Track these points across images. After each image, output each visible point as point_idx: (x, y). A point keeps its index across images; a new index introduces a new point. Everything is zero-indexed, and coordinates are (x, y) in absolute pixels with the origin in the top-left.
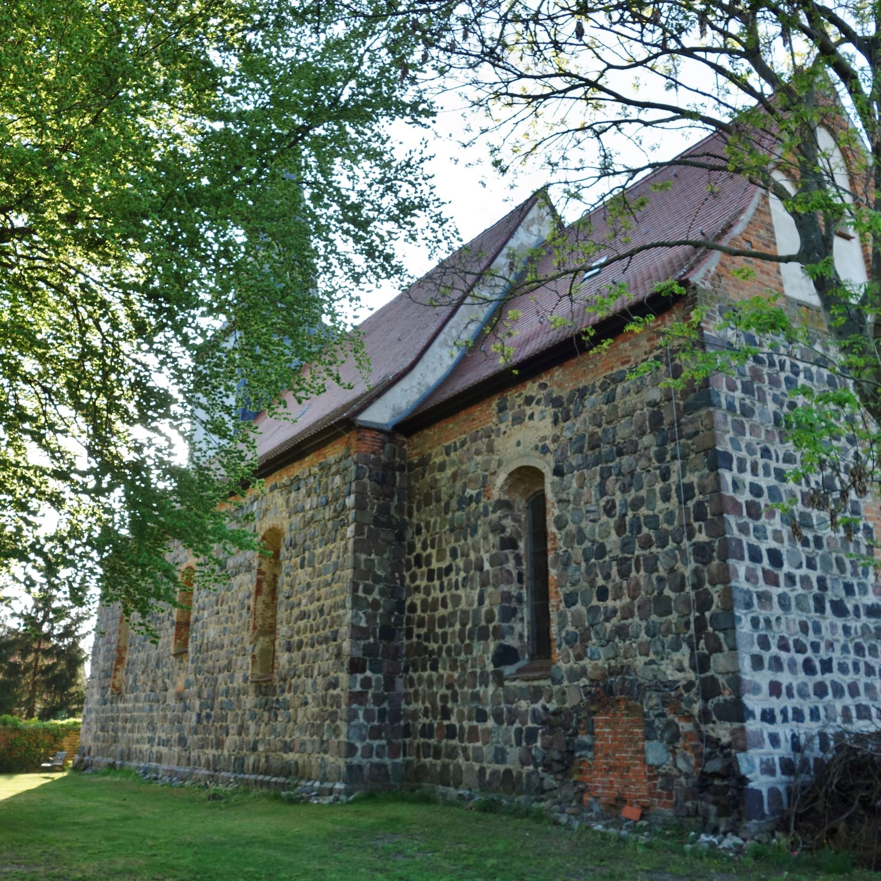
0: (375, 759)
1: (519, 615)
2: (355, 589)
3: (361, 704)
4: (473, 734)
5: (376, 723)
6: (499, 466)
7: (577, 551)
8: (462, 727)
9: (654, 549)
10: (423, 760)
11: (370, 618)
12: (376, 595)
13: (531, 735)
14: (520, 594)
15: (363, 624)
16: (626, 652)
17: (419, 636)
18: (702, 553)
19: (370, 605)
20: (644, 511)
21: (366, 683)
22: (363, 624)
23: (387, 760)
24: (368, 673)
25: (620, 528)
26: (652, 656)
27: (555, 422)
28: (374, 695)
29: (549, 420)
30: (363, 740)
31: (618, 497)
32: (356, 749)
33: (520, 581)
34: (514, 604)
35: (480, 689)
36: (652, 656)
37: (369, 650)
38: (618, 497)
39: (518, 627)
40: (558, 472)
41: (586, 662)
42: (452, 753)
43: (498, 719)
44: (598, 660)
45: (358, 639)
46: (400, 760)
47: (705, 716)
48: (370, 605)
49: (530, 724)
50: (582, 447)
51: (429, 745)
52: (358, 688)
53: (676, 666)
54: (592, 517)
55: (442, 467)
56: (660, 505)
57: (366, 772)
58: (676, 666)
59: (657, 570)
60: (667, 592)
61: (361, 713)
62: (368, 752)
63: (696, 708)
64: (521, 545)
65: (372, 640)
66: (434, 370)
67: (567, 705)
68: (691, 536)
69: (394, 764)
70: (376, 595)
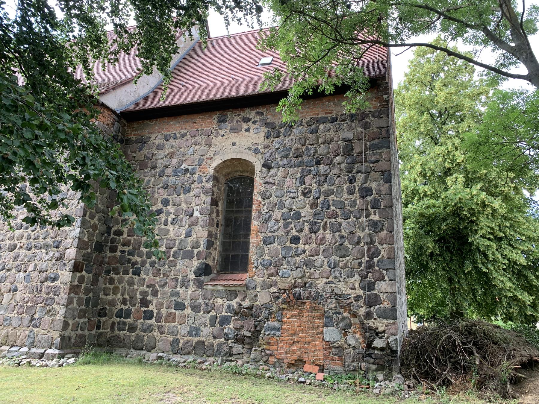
0: (79, 332)
1: (215, 246)
2: (84, 215)
3: (76, 293)
4: (171, 318)
5: (83, 307)
6: (215, 155)
7: (277, 214)
8: (159, 313)
9: (338, 220)
10: (117, 332)
11: (91, 235)
12: (96, 220)
13: (225, 321)
14: (216, 234)
15: (86, 239)
16: (311, 275)
17: (123, 252)
18: (375, 226)
19: (91, 227)
20: (332, 198)
21: (82, 279)
22: (86, 239)
23: (86, 332)
24: (84, 273)
25: (313, 205)
26: (331, 279)
27: (268, 136)
28: (85, 288)
29: (262, 135)
30: (74, 319)
31: (314, 187)
32: (69, 324)
33: (217, 226)
34: (213, 239)
35: (182, 290)
36: (331, 279)
37: (87, 257)
38: (314, 187)
39: (213, 253)
40: (267, 166)
41: (277, 278)
42: (148, 329)
43: (196, 308)
44: (287, 276)
45: (81, 249)
46: (94, 332)
47: (369, 315)
48: (91, 227)
49: (224, 313)
50: (288, 154)
51: (124, 324)
52: (76, 283)
53: (350, 287)
54: (292, 195)
55: (160, 147)
56: (346, 196)
57: (73, 340)
58: (350, 287)
59: (340, 231)
60: (346, 244)
61: (75, 300)
62: (76, 327)
63: (362, 311)
64: (220, 204)
65: (89, 250)
66: (144, 87)
67: (258, 303)
68: (367, 216)
69: (90, 334)
70: (96, 220)
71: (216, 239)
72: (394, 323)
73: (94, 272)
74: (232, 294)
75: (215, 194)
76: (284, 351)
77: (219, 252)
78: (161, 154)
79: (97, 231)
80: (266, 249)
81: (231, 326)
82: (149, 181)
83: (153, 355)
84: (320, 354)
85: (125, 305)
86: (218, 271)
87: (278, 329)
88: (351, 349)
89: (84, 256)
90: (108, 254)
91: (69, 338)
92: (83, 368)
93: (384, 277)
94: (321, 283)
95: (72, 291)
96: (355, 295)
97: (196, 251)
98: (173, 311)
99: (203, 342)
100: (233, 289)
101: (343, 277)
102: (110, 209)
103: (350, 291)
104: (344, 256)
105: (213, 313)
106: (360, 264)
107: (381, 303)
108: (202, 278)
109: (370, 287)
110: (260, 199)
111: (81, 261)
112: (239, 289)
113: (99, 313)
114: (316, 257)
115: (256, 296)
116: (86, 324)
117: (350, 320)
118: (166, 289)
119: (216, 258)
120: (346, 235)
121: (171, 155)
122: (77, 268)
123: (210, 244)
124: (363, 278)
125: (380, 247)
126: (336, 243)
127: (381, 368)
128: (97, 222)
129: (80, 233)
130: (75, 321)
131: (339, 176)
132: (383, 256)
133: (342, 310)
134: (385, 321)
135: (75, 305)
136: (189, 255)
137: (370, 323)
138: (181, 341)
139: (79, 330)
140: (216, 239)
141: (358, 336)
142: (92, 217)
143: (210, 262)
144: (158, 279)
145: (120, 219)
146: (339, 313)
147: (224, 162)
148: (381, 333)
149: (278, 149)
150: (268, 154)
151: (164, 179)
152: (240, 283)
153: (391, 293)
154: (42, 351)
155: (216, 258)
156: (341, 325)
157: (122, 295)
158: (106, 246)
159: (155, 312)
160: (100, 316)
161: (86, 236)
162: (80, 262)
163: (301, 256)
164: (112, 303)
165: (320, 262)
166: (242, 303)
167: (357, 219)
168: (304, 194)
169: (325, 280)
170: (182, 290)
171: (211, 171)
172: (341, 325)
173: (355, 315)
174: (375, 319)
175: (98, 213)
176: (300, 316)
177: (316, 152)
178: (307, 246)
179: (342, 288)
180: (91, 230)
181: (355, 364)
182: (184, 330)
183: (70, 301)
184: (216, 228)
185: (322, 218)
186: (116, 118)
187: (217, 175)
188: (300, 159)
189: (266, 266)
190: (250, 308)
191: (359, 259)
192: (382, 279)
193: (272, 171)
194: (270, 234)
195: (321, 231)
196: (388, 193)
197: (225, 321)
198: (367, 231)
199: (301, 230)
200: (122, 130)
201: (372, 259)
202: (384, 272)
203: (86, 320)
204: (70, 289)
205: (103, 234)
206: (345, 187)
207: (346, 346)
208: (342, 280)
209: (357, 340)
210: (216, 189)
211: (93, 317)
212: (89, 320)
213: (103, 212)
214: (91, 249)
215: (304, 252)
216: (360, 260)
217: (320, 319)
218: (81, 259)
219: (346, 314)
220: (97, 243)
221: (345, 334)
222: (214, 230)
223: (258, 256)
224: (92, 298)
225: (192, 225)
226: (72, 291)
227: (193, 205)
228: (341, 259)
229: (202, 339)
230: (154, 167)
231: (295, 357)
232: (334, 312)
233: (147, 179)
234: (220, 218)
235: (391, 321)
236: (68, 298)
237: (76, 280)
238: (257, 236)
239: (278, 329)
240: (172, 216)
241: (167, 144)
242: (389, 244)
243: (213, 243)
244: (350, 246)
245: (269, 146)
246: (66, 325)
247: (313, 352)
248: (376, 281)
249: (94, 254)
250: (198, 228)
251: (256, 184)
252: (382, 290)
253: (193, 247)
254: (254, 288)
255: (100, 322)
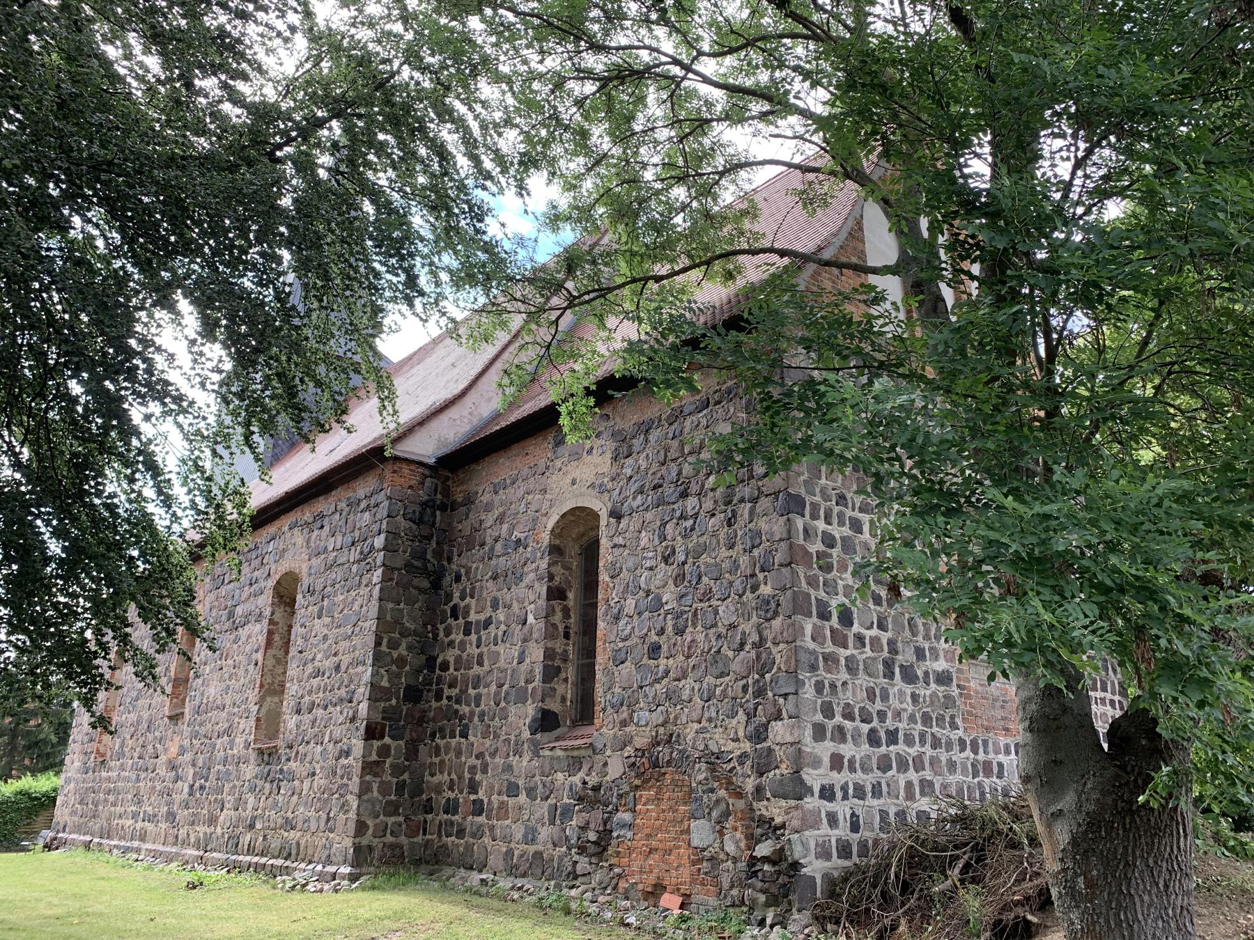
0: (389, 839)
1: (563, 675)
2: (378, 643)
5: (393, 797)
10: (444, 838)
11: (394, 677)
12: (402, 650)
14: (565, 651)
15: (385, 683)
16: (676, 718)
17: (449, 698)
19: (393, 662)
21: (384, 752)
22: (385, 683)
23: (403, 840)
24: (387, 740)
26: (704, 723)
30: (377, 817)
32: (367, 827)
34: (557, 663)
35: (514, 760)
37: (389, 714)
39: (561, 689)
40: (616, 515)
42: (478, 833)
43: (531, 792)
45: (376, 700)
49: (566, 800)
51: (452, 823)
52: (374, 757)
53: (729, 737)
61: (375, 787)
62: (382, 831)
63: (750, 785)
64: (571, 595)
65: (394, 702)
68: (755, 588)
70: (402, 650)
71: (565, 661)
72: (796, 807)
73: (407, 736)
74: (574, 764)
75: (557, 578)
76: (640, 870)
77: (575, 684)
78: (489, 519)
79: (408, 668)
80: (616, 674)
81: (574, 823)
82: (477, 568)
83: (476, 877)
84: (686, 873)
85: (453, 791)
86: (572, 722)
87: (630, 826)
88: (729, 862)
89: (384, 711)
90: (434, 704)
91: (370, 848)
92: (360, 894)
93: (780, 711)
94: (690, 731)
95: (367, 770)
96: (739, 753)
97: (530, 687)
98: (506, 798)
99: (541, 853)
100: (576, 753)
101: (721, 717)
102: (429, 627)
103: (731, 746)
104: (722, 675)
105: (551, 801)
106: (745, 689)
107: (777, 767)
108: (538, 736)
109: (759, 735)
110: (607, 579)
111: (379, 720)
112: (583, 753)
113: (425, 806)
114: (683, 682)
115: (605, 764)
116: (400, 825)
117: (728, 804)
118: (497, 760)
119: (569, 696)
120: (724, 631)
121: (501, 519)
122: (372, 733)
123: (551, 673)
124: (750, 716)
125: (774, 650)
126: (710, 649)
127: (773, 901)
128: (405, 653)
129: (372, 675)
130: (378, 821)
131: (713, 515)
132: (779, 668)
133: (716, 784)
134: (783, 803)
135: (376, 793)
136: (522, 699)
137: (762, 808)
138: (516, 853)
139: (388, 835)
140: (565, 661)
141: (738, 835)
142: (394, 645)
143: (554, 706)
144: (488, 742)
145: (446, 640)
146: (712, 791)
147: (563, 516)
148: (779, 829)
149: (631, 477)
150: (617, 491)
151: (493, 562)
152: (585, 741)
153: (792, 744)
154: (88, 838)
155: (569, 696)
156: (715, 814)
157: (449, 775)
158: (429, 691)
159: (486, 801)
160: (427, 813)
161: (386, 678)
162: (377, 723)
163: (664, 682)
164: (438, 789)
165: (687, 692)
166: (587, 779)
167: (740, 596)
168: (666, 559)
169: (696, 726)
170: (514, 760)
171: (545, 538)
172: (715, 814)
173: (739, 795)
174: (768, 799)
175: (405, 637)
176: (658, 799)
177: (680, 473)
178: (671, 661)
179: (719, 740)
180: (394, 668)
181: (735, 892)
182: (518, 832)
183: (365, 789)
184: (565, 641)
185: (689, 603)
186: (427, 472)
187: (557, 542)
188: (660, 490)
189: (617, 708)
190: (596, 789)
191: (743, 677)
192: (778, 717)
193: (624, 522)
194: (621, 645)
195: (690, 629)
196: (785, 536)
197: (567, 813)
198: (755, 619)
199: (661, 632)
200: (443, 489)
201: (762, 676)
202: (781, 700)
203: (401, 819)
204: (363, 768)
205: (419, 671)
206: (722, 534)
207: (722, 856)
208: (719, 723)
209: (737, 843)
210: (557, 570)
211: (414, 813)
212: (407, 819)
213: (415, 633)
214: (398, 699)
215: (667, 672)
216: (744, 681)
217: (685, 804)
218: (378, 718)
219: (722, 793)
220: (408, 688)
221: (721, 833)
222: (558, 645)
223: (606, 688)
224: (408, 781)
225: (525, 640)
226: (367, 770)
227: (526, 603)
228: (718, 681)
229: (540, 848)
230: (482, 544)
231: (652, 879)
232: (705, 788)
233: (475, 566)
234: (572, 621)
235: (793, 803)
236: (361, 783)
237: (374, 753)
238: (605, 649)
239: (630, 826)
240: (503, 628)
241: (497, 499)
242: (787, 642)
243: (558, 670)
244: (730, 654)
245: (618, 475)
246: (361, 827)
247: (677, 869)
248: (769, 722)
249: (405, 708)
250: (532, 644)
251: (602, 551)
252: (779, 739)
253: (527, 682)
254: (602, 751)
255: (425, 821)
